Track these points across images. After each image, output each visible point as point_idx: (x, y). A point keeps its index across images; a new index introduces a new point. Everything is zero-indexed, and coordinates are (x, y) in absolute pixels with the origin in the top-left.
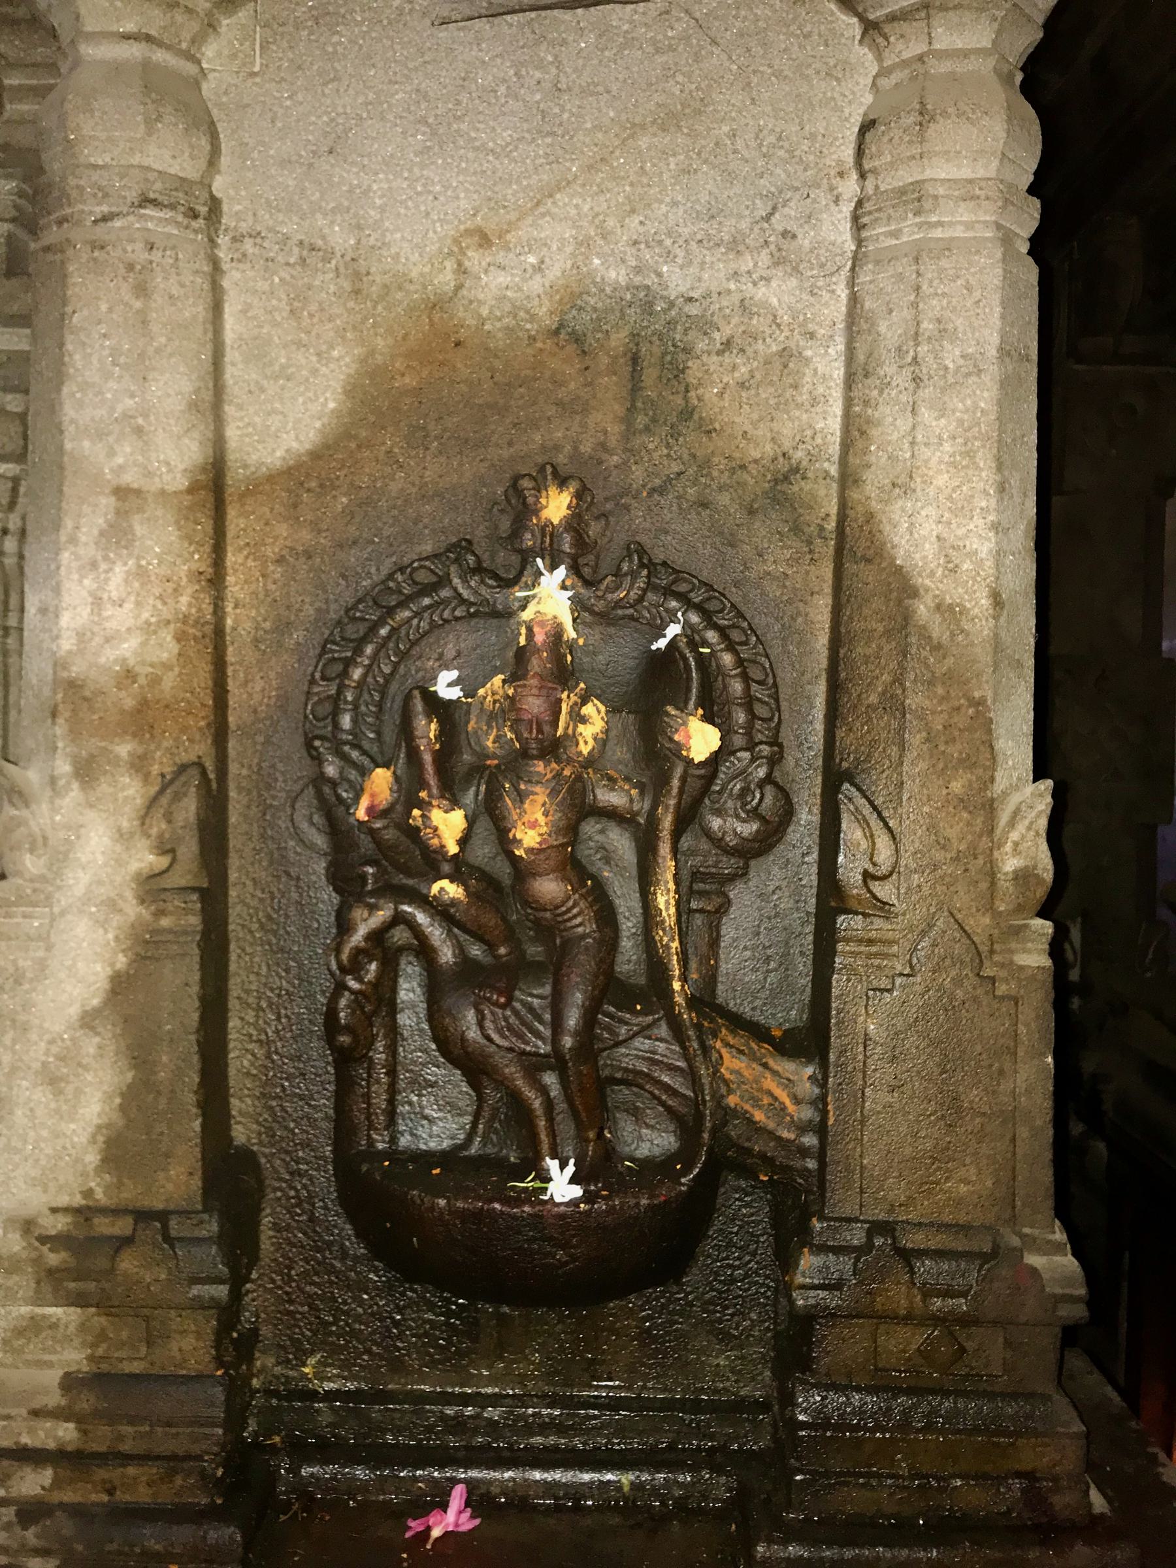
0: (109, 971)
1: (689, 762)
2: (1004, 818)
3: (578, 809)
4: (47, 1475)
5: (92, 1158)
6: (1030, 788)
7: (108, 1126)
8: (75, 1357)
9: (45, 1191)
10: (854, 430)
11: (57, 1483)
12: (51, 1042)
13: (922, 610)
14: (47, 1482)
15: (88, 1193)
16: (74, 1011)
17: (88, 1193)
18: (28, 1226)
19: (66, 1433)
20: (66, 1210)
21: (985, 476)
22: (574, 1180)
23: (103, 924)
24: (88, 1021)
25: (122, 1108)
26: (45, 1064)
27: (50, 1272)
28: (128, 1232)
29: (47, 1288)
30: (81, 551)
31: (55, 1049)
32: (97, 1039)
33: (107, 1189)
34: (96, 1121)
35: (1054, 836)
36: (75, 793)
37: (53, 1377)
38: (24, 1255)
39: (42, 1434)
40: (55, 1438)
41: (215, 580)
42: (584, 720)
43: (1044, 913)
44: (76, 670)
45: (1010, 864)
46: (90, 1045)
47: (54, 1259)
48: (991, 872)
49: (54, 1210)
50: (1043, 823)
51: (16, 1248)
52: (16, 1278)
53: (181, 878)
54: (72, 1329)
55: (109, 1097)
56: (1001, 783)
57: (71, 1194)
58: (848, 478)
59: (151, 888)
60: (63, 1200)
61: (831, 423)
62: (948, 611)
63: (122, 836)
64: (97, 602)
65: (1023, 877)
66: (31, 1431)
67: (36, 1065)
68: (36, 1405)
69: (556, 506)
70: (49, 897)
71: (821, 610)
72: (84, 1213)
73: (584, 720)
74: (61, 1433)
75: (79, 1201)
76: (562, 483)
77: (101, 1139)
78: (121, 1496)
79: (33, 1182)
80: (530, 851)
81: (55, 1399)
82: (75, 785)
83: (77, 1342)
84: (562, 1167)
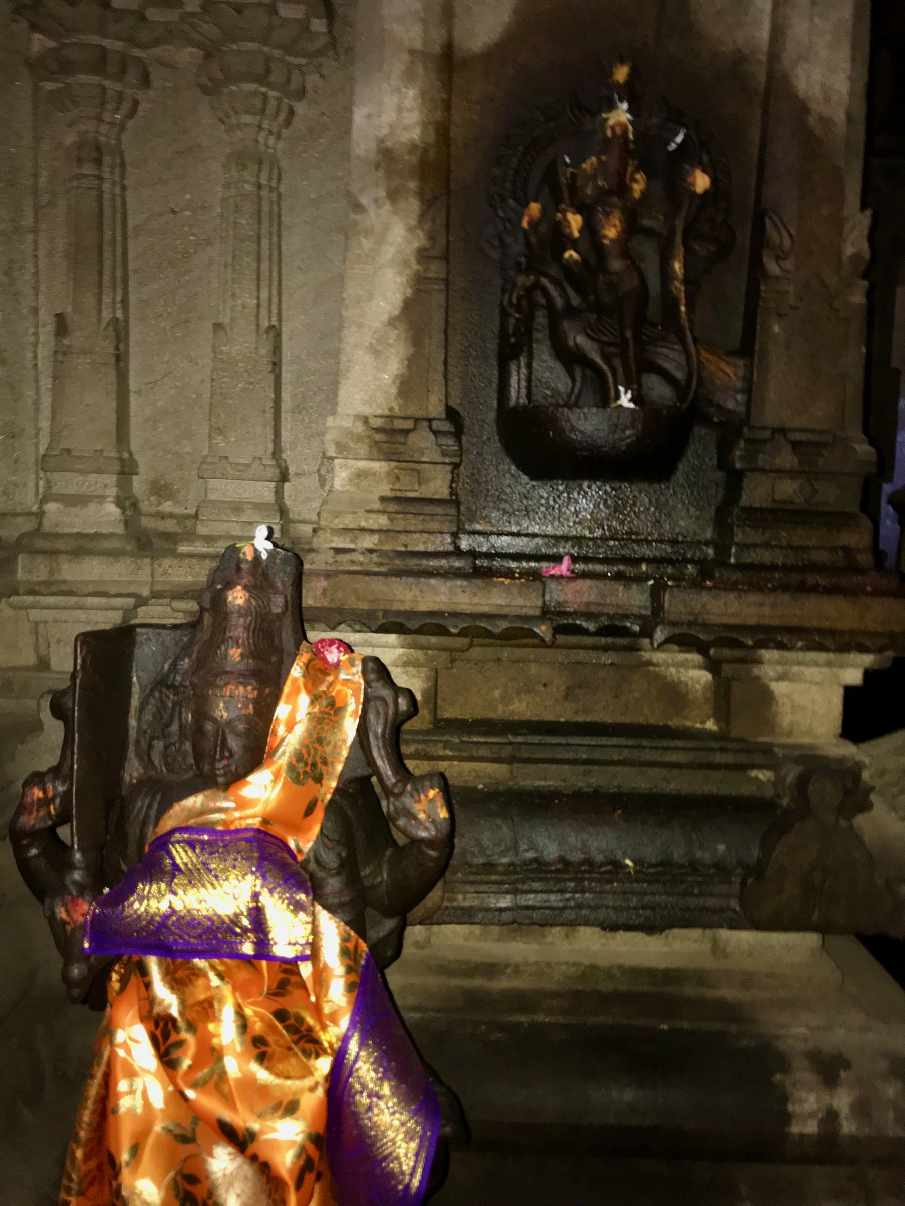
0: (403, 297)
1: (694, 193)
2: (846, 228)
3: (631, 229)
4: (376, 538)
5: (394, 391)
6: (859, 216)
7: (402, 376)
8: (385, 489)
9: (371, 407)
10: (778, 32)
11: (380, 542)
12: (375, 332)
13: (812, 120)
14: (376, 541)
15: (391, 409)
16: (385, 317)
17: (391, 409)
18: (365, 420)
19: (383, 521)
20: (381, 416)
21: (845, 52)
22: (631, 401)
23: (400, 273)
24: (392, 322)
25: (409, 367)
26: (371, 344)
27: (376, 442)
28: (411, 427)
29: (375, 450)
30: (393, 82)
31: (376, 336)
32: (397, 332)
33: (400, 406)
34: (396, 372)
35: (871, 239)
36: (387, 207)
37: (376, 496)
38: (364, 433)
39: (371, 521)
40: (378, 523)
41: (448, 106)
42: (636, 181)
43: (865, 276)
44: (389, 144)
45: (849, 250)
46: (393, 334)
47: (378, 437)
48: (839, 254)
49: (376, 416)
50: (866, 231)
51: (360, 430)
52: (360, 445)
53: (436, 252)
54: (383, 475)
55: (402, 361)
56: (846, 212)
57: (383, 409)
58: (774, 56)
59: (423, 255)
60: (379, 412)
61: (764, 34)
62: (826, 122)
63: (411, 230)
64: (400, 109)
65: (856, 257)
66: (366, 519)
67: (366, 344)
68: (367, 508)
69: (622, 74)
70: (374, 259)
71: (754, 134)
72: (390, 418)
73: (636, 181)
74: (380, 521)
75: (386, 412)
76: (622, 61)
77: (398, 382)
78: (409, 549)
79: (364, 403)
80: (611, 240)
81: (377, 506)
82: (388, 203)
83: (386, 481)
84: (626, 393)
